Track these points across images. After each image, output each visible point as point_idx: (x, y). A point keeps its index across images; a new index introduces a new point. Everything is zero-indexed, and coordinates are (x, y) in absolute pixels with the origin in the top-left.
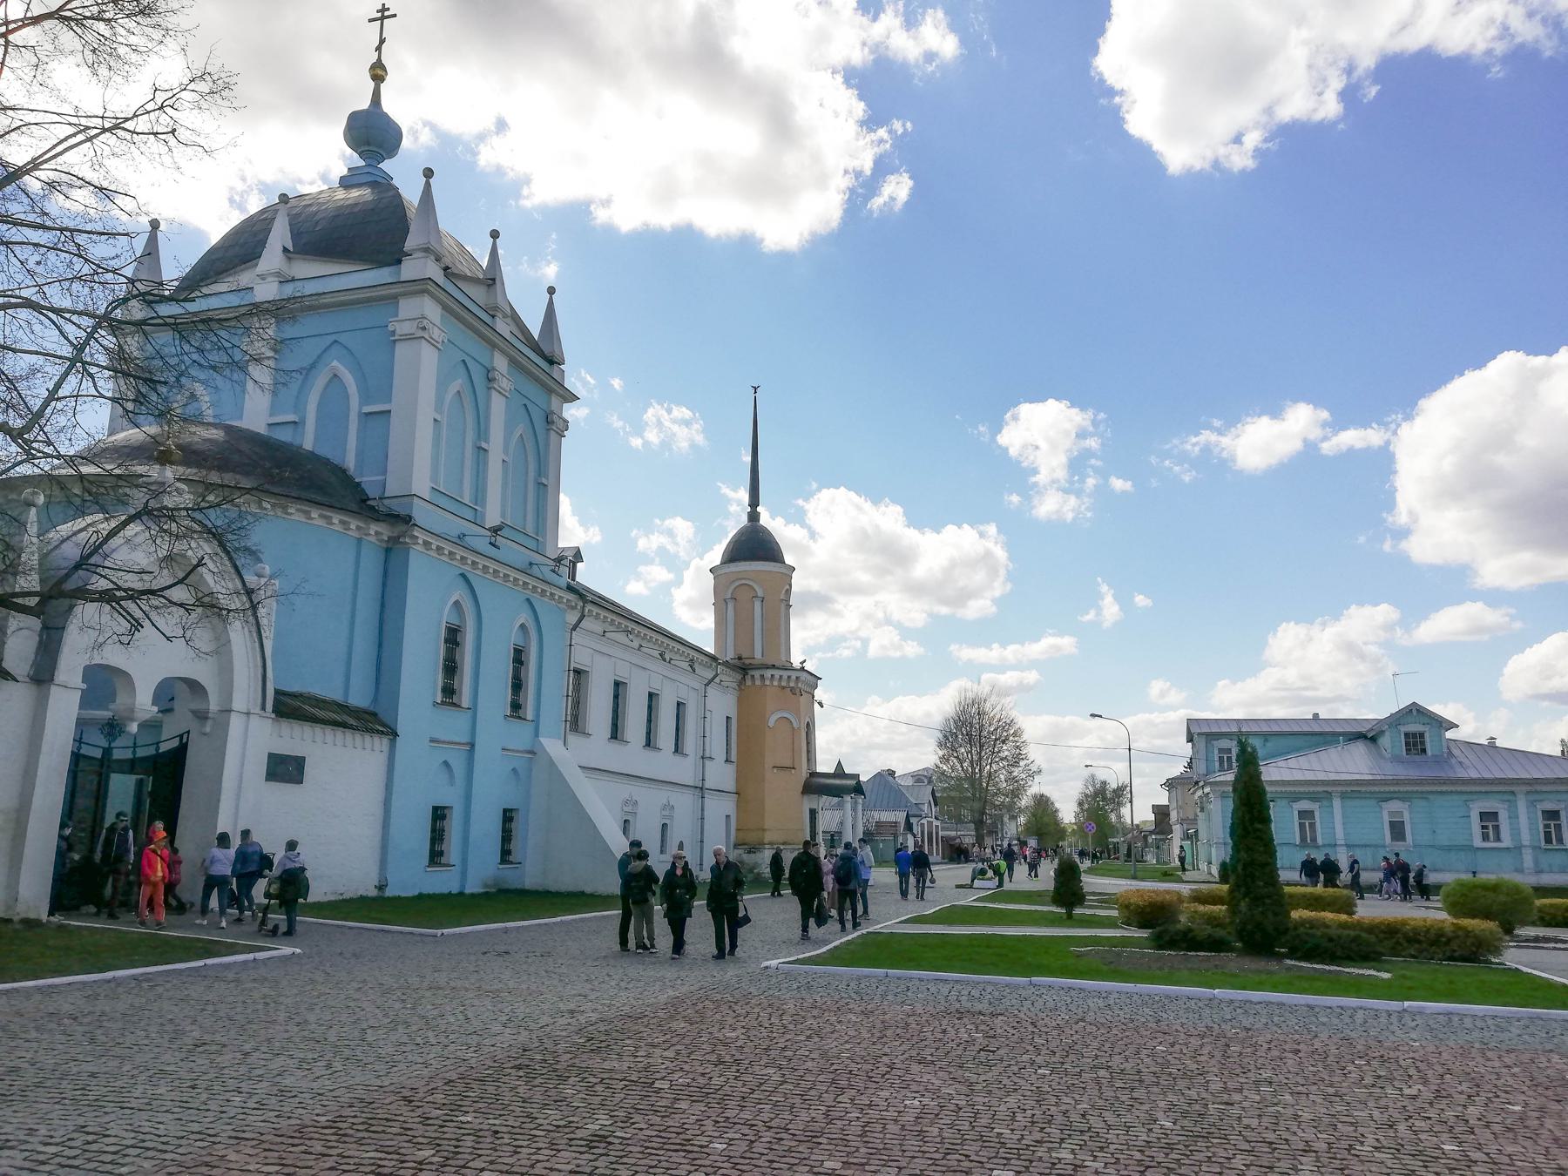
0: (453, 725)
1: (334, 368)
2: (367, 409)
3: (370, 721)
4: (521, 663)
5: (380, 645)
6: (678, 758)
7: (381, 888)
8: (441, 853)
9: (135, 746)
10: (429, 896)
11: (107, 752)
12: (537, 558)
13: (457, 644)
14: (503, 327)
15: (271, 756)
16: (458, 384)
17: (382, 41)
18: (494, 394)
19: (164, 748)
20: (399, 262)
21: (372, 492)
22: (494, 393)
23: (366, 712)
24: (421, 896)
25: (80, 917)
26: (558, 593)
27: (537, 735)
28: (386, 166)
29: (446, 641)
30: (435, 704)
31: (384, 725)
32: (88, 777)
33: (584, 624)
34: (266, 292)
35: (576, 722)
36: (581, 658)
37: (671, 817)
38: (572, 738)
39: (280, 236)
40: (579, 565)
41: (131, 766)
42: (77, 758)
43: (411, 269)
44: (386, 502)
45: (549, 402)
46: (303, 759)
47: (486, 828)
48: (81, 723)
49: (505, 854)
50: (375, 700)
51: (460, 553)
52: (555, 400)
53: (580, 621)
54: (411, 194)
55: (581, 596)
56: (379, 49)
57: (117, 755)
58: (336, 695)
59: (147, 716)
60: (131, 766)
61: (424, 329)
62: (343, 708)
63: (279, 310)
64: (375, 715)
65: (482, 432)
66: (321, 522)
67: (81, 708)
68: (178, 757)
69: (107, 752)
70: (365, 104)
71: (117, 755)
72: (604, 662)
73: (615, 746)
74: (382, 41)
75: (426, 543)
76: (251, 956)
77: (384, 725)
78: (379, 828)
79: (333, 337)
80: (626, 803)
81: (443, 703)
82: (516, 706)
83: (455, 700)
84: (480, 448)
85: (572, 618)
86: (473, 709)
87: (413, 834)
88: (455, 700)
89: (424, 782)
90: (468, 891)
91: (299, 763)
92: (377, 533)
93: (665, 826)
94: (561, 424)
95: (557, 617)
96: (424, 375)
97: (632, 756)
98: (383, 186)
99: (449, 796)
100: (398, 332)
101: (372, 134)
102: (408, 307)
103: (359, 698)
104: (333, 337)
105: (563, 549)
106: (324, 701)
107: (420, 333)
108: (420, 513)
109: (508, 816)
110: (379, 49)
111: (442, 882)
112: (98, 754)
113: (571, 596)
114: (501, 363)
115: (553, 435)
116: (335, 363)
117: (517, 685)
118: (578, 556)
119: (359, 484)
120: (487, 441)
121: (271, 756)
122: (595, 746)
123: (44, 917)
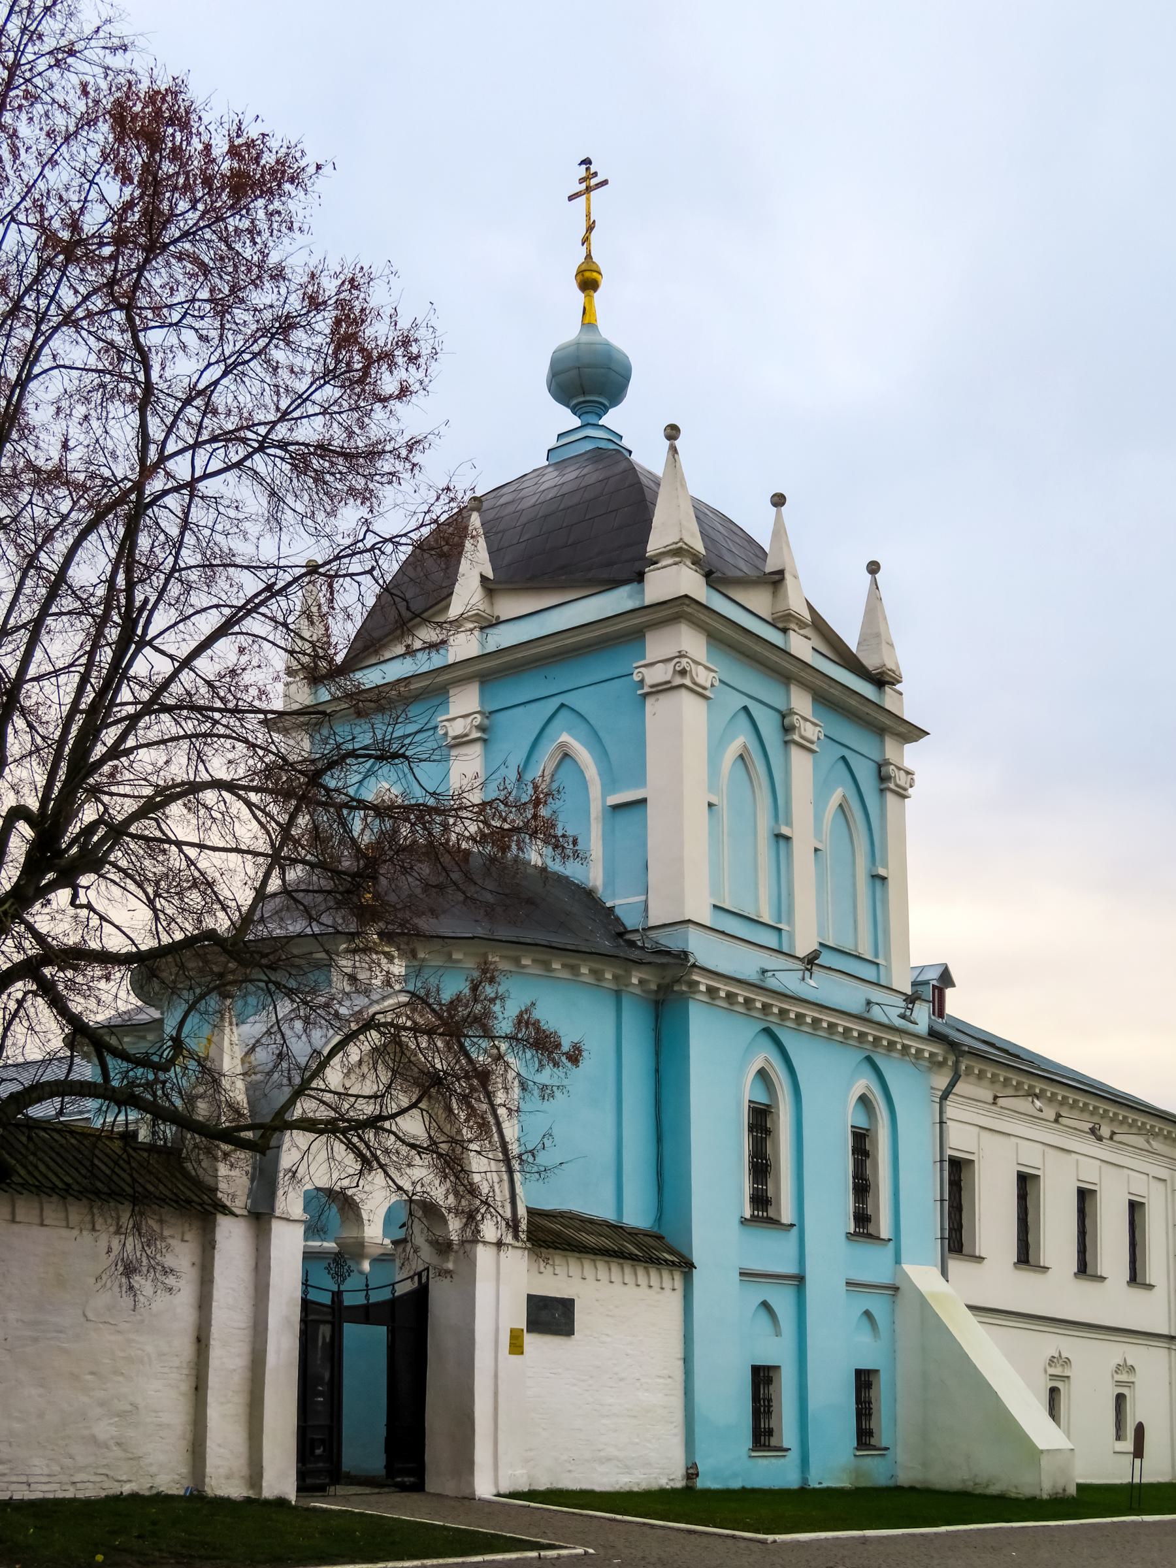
0: (772, 1252)
1: (563, 745)
2: (614, 799)
3: (654, 1250)
4: (866, 1154)
5: (659, 1140)
6: (1137, 1294)
7: (692, 1474)
8: (770, 1432)
9: (367, 1288)
10: (754, 1491)
11: (337, 1295)
12: (877, 995)
13: (768, 1132)
14: (801, 646)
15: (531, 1298)
16: (742, 739)
17: (590, 228)
18: (795, 752)
19: (401, 1289)
20: (640, 578)
21: (631, 921)
22: (794, 750)
23: (646, 1234)
24: (744, 1490)
25: (325, 1497)
26: (914, 1045)
27: (898, 1261)
28: (612, 419)
29: (751, 1130)
30: (744, 1222)
31: (672, 1252)
32: (321, 1323)
33: (960, 1088)
34: (465, 646)
35: (956, 1240)
36: (960, 1141)
37: (1130, 1384)
38: (954, 1265)
39: (475, 563)
40: (949, 992)
41: (367, 1314)
42: (306, 1305)
43: (663, 583)
44: (653, 934)
45: (882, 750)
46: (571, 1302)
47: (832, 1396)
48: (309, 1256)
49: (865, 1437)
50: (659, 1219)
51: (760, 1000)
52: (891, 749)
53: (952, 1084)
54: (648, 456)
55: (953, 1046)
56: (586, 240)
57: (349, 1300)
58: (605, 1212)
59: (380, 1251)
60: (367, 1314)
61: (683, 673)
62: (617, 1229)
63: (491, 671)
64: (660, 1238)
65: (780, 809)
66: (565, 974)
67: (306, 1239)
68: (421, 1296)
69: (337, 1295)
70: (569, 332)
71: (349, 1300)
72: (1000, 1142)
73: (1027, 1277)
74: (590, 228)
75: (712, 991)
76: (534, 1554)
77: (672, 1252)
78: (679, 1392)
79: (554, 703)
80: (1052, 1361)
81: (754, 1219)
82: (863, 1219)
83: (771, 1213)
84: (779, 837)
85: (941, 1081)
86: (799, 1225)
87: (729, 1405)
88: (771, 1213)
89: (735, 1336)
90: (813, 1484)
91: (567, 1305)
92: (641, 981)
93: (1054, 1391)
94: (902, 779)
95: (912, 1090)
96: (689, 740)
97: (1056, 1290)
98: (612, 457)
99: (775, 1350)
100: (649, 681)
101: (589, 381)
102: (658, 645)
103: (637, 1214)
104: (554, 703)
105: (923, 969)
106: (592, 1222)
107: (678, 681)
108: (705, 950)
109: (864, 1380)
110: (586, 240)
111: (774, 1472)
112: (326, 1299)
113: (937, 1049)
114: (801, 702)
115: (890, 798)
116: (565, 737)
117: (862, 1187)
118: (946, 979)
119: (611, 909)
120: (789, 823)
121: (531, 1298)
122: (994, 1275)
123: (292, 1496)
